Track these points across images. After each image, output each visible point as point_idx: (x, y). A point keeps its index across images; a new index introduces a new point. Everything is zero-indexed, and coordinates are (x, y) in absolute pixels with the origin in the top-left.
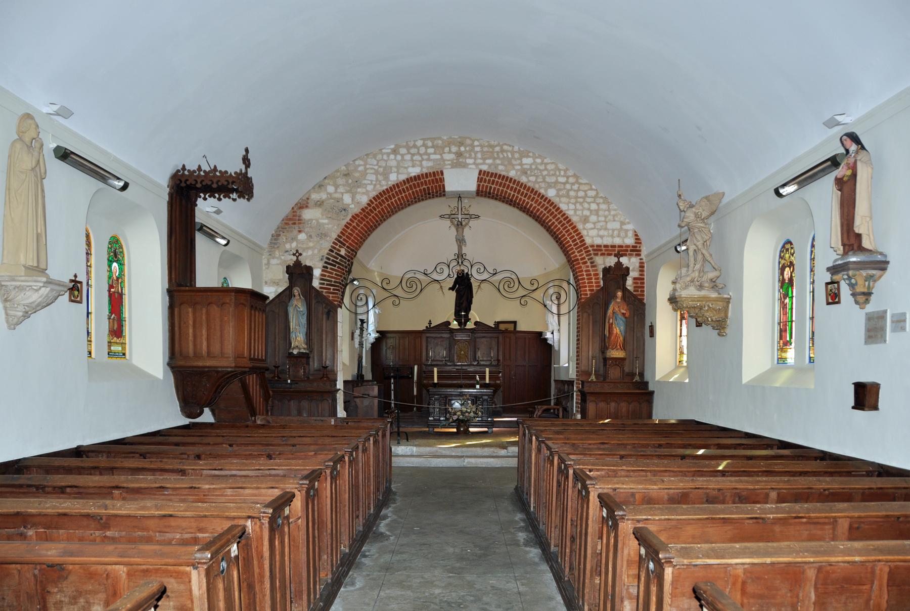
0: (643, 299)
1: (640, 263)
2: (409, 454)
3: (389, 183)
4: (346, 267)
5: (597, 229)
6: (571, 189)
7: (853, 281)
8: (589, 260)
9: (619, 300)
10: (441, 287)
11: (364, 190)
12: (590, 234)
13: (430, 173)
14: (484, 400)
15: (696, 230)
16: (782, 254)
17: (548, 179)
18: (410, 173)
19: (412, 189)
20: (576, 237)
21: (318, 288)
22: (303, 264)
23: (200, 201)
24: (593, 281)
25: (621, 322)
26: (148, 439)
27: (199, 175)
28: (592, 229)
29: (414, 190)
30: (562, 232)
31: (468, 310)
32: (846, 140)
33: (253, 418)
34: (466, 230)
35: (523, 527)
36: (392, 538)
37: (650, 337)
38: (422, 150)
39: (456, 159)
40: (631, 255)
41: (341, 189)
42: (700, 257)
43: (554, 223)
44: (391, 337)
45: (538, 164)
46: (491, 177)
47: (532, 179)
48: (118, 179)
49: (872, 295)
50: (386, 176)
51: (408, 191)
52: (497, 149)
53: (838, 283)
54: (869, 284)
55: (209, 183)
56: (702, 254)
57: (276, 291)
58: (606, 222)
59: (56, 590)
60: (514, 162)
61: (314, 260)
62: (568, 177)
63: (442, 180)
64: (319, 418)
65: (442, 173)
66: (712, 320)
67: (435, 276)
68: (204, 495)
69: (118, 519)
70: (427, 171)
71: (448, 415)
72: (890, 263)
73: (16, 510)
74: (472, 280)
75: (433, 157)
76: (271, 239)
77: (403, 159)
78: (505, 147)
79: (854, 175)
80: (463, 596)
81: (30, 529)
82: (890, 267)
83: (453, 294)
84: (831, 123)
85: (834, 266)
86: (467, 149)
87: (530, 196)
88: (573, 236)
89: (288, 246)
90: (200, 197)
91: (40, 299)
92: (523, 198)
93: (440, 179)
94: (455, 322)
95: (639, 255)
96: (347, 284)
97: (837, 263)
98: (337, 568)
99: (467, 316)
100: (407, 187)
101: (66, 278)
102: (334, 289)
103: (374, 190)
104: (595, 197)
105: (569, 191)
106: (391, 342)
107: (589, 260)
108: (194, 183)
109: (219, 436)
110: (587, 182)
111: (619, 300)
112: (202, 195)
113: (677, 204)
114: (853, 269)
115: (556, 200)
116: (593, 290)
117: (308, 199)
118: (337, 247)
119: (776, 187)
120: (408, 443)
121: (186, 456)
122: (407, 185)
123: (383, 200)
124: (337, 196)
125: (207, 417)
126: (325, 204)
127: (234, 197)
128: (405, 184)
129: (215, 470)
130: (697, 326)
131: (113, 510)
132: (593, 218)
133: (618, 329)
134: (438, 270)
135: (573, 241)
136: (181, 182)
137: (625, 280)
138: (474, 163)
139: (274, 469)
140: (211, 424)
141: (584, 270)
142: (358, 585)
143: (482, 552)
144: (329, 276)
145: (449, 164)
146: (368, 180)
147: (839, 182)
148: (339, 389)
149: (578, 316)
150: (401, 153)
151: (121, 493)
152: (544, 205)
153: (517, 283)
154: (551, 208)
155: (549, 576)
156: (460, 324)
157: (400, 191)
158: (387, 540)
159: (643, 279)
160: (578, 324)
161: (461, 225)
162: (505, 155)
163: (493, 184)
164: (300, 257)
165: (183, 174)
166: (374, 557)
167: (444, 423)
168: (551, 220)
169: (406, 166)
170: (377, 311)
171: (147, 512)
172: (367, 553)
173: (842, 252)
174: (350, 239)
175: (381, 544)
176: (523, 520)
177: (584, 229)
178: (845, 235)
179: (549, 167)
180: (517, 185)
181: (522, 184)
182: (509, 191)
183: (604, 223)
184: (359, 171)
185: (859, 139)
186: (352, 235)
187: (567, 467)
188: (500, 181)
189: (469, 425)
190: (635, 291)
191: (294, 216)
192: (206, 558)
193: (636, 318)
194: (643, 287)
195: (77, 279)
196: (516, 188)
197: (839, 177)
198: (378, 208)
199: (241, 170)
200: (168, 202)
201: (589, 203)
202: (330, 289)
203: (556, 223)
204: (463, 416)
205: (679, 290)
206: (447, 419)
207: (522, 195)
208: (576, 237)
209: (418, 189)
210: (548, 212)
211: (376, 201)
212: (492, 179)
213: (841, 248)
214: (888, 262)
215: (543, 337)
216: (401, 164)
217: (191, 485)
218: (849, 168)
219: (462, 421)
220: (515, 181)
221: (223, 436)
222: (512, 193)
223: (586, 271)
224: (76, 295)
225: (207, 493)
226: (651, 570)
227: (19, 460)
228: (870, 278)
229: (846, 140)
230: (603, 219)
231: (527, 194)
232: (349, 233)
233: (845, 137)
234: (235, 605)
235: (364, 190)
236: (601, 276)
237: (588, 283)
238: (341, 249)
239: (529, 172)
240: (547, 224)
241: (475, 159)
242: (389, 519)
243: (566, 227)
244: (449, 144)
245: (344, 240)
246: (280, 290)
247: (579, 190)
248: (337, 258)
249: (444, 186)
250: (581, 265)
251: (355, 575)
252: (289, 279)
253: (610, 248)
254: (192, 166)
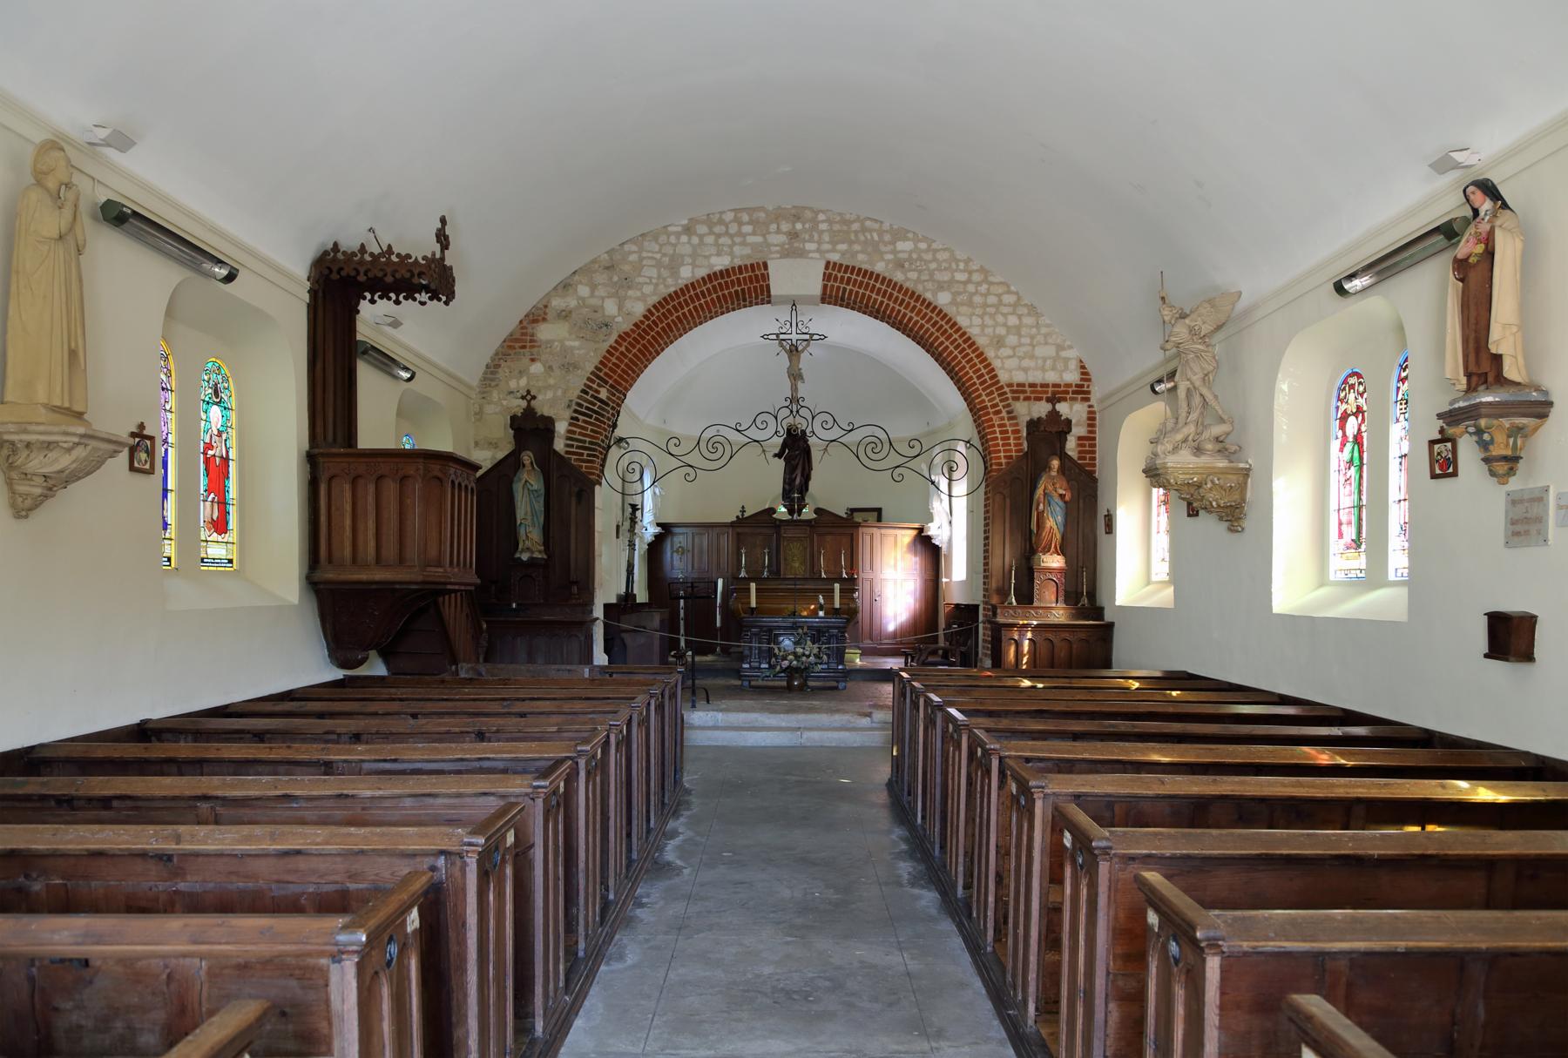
0: (1094, 472)
1: (1090, 412)
2: (711, 724)
3: (680, 281)
4: (609, 419)
5: (1019, 357)
6: (976, 292)
7: (1486, 437)
8: (1004, 407)
9: (1054, 473)
10: (764, 451)
11: (639, 294)
12: (1006, 366)
13: (746, 266)
14: (831, 636)
15: (1192, 356)
16: (1342, 395)
17: (939, 276)
18: (714, 266)
19: (716, 292)
20: (983, 371)
21: (562, 453)
22: (539, 414)
23: (364, 306)
24: (1012, 441)
25: (1058, 509)
26: (269, 707)
27: (362, 262)
28: (1010, 357)
29: (720, 293)
30: (960, 362)
31: (804, 488)
32: (1473, 193)
33: (454, 667)
34: (804, 356)
35: (906, 852)
36: (686, 871)
37: (1107, 533)
38: (733, 228)
39: (789, 244)
40: (1073, 399)
41: (601, 292)
42: (1197, 400)
43: (947, 347)
44: (680, 534)
45: (923, 251)
46: (845, 272)
47: (913, 275)
48: (219, 262)
49: (1521, 461)
50: (674, 269)
51: (710, 294)
52: (856, 226)
53: (1453, 441)
54: (1515, 443)
55: (380, 274)
56: (1201, 395)
57: (493, 457)
58: (1034, 346)
59: (69, 1005)
60: (883, 248)
61: (556, 402)
62: (970, 273)
63: (765, 277)
64: (563, 667)
65: (766, 266)
66: (1219, 506)
67: (754, 433)
68: (363, 809)
69: (200, 859)
70: (740, 263)
71: (773, 659)
72: (1555, 405)
73: (9, 847)
74: (812, 441)
75: (750, 239)
76: (485, 373)
77: (701, 242)
78: (868, 223)
79: (1490, 254)
80: (812, 979)
81: (36, 880)
82: (1554, 413)
83: (781, 463)
84: (1443, 164)
85: (1450, 411)
86: (807, 226)
87: (909, 303)
88: (979, 369)
89: (513, 384)
90: (365, 298)
91: (74, 465)
92: (897, 307)
93: (763, 275)
94: (783, 509)
95: (1088, 400)
96: (609, 447)
97: (1456, 406)
98: (595, 931)
100: (708, 289)
101: (122, 429)
102: (588, 455)
103: (654, 294)
104: (1015, 306)
105: (972, 295)
106: (680, 539)
107: (1004, 407)
108: (353, 273)
109: (394, 700)
110: (1002, 280)
111: (1054, 473)
112: (368, 296)
113: (1160, 311)
114: (1488, 416)
115: (951, 311)
116: (1011, 457)
117: (546, 307)
118: (595, 386)
119: (1337, 279)
120: (710, 706)
121: (335, 737)
122: (709, 285)
123: (669, 310)
124: (593, 302)
125: (376, 668)
126: (574, 315)
127: (423, 300)
128: (705, 283)
129: (385, 761)
130: (1189, 515)
131: (191, 843)
132: (1012, 340)
133: (1053, 522)
134: (758, 422)
135: (978, 378)
136: (331, 271)
137: (1063, 441)
138: (818, 250)
139: (488, 759)
140: (382, 678)
141: (996, 424)
142: (631, 958)
143: (838, 896)
144: (580, 434)
145: (777, 252)
146: (644, 276)
147: (1461, 266)
148: (597, 619)
149: (986, 499)
150: (698, 232)
151: (212, 807)
152: (931, 318)
153: (887, 446)
154: (943, 323)
155: (957, 942)
156: (791, 512)
157: (697, 295)
158: (678, 875)
159: (1094, 439)
160: (987, 512)
161: (797, 350)
162: (869, 237)
163: (848, 284)
164: (533, 402)
165: (335, 259)
166: (657, 906)
167: (768, 674)
168: (942, 343)
169: (707, 254)
170: (657, 491)
171: (254, 847)
172: (644, 900)
173: (1465, 387)
174: (615, 372)
175: (668, 883)
176: (905, 840)
177: (997, 357)
178: (1472, 358)
179: (940, 256)
180: (888, 286)
181: (896, 284)
182: (874, 296)
183: (1030, 348)
184: (631, 262)
185: (1497, 191)
186: (618, 367)
187: (987, 753)
188: (860, 279)
189: (807, 677)
190: (1080, 458)
191: (523, 334)
192: (359, 943)
193: (1081, 501)
194: (1094, 452)
195: (145, 432)
196: (886, 291)
197: (1460, 256)
198: (662, 322)
199: (434, 254)
200: (309, 305)
201: (1005, 315)
202: (582, 454)
203: (951, 348)
204: (798, 661)
205: (1162, 456)
206: (772, 667)
207: (895, 302)
208: (983, 371)
209: (726, 292)
210: (938, 330)
211: (658, 311)
212: (846, 276)
213: (1464, 380)
214: (1551, 404)
216: (699, 251)
217: (339, 792)
218: (1479, 241)
219: (797, 669)
220: (884, 278)
221: (401, 700)
222: (880, 299)
223: (1000, 426)
224: (143, 459)
225: (368, 805)
226: (1174, 958)
227: (33, 748)
228: (1516, 431)
229: (1473, 193)
230: (1027, 341)
231: (903, 300)
232: (614, 364)
233: (1471, 188)
234: (411, 1022)
235: (639, 294)
236: (1025, 434)
237: (1003, 445)
238: (601, 389)
239: (907, 265)
240: (936, 348)
241: (819, 243)
242: (681, 837)
243: (968, 354)
244: (776, 219)
245: (606, 374)
246: (500, 455)
247: (988, 293)
248: (594, 405)
249: (768, 286)
250: (991, 416)
251: (625, 941)
252: (514, 437)
253: (1039, 389)
254: (350, 243)
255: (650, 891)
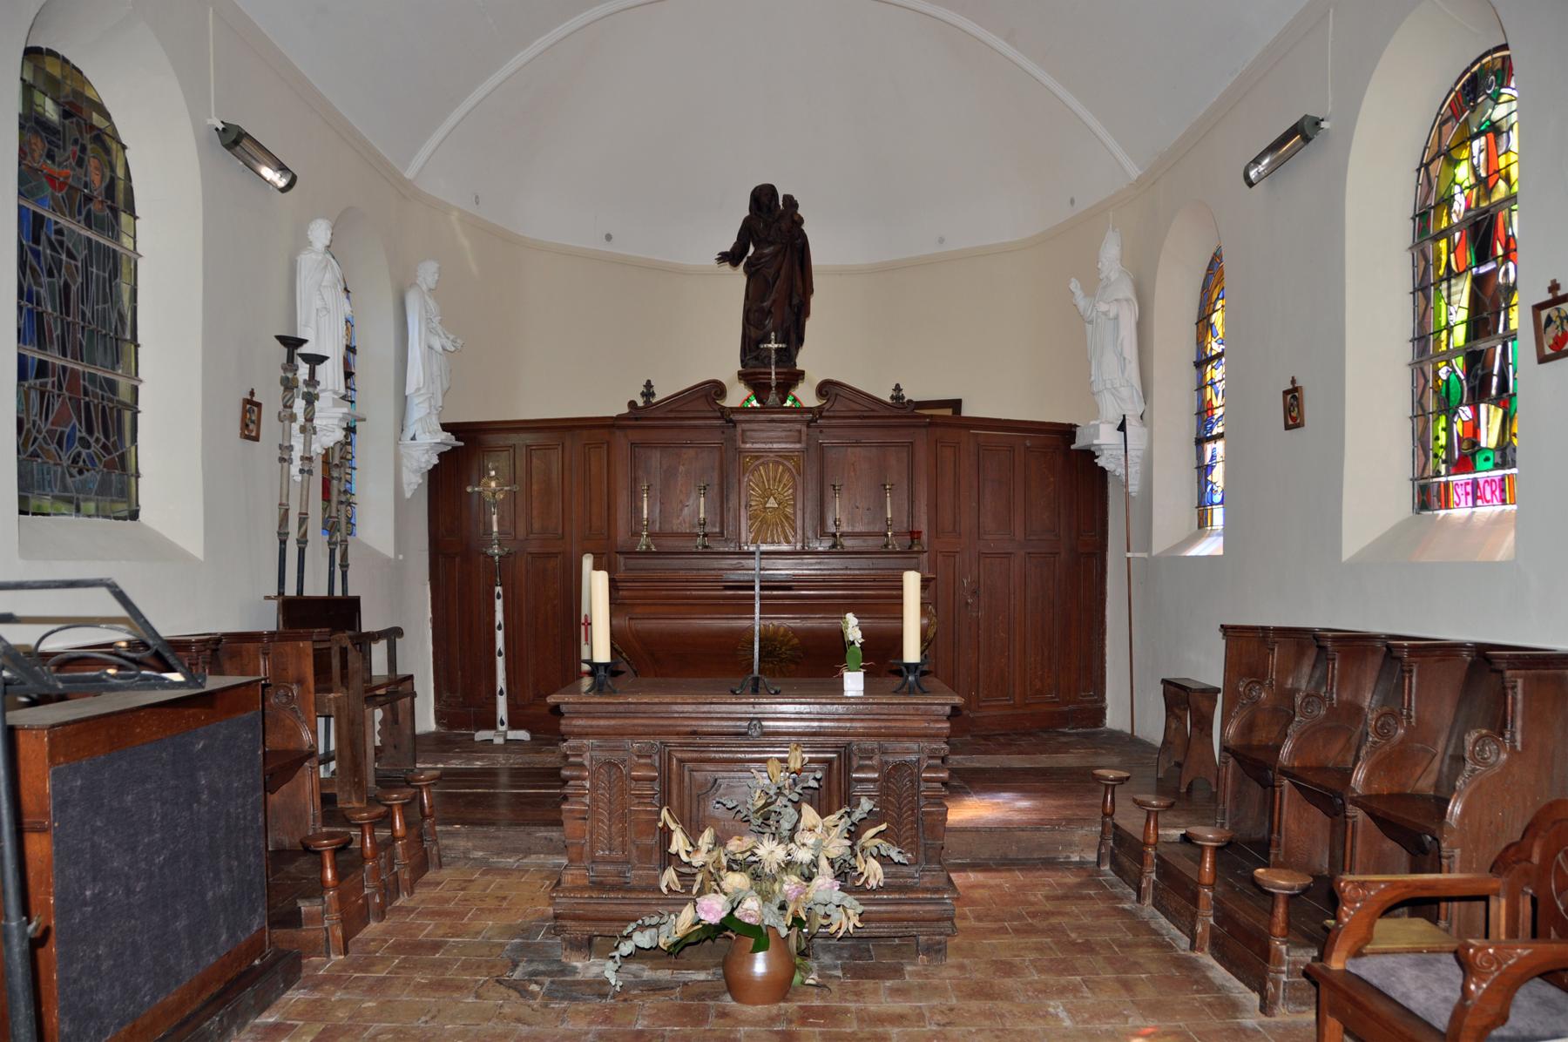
31: (794, 336)
83: (736, 281)
99: (787, 357)
195: (254, 399)
215: (1079, 443)
255: (903, 961)
